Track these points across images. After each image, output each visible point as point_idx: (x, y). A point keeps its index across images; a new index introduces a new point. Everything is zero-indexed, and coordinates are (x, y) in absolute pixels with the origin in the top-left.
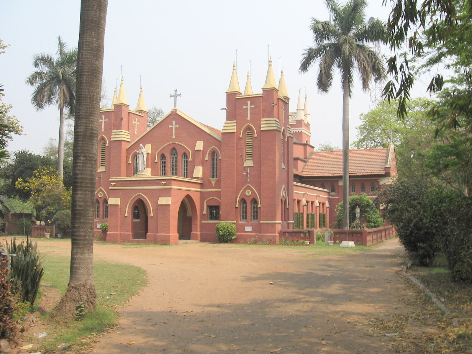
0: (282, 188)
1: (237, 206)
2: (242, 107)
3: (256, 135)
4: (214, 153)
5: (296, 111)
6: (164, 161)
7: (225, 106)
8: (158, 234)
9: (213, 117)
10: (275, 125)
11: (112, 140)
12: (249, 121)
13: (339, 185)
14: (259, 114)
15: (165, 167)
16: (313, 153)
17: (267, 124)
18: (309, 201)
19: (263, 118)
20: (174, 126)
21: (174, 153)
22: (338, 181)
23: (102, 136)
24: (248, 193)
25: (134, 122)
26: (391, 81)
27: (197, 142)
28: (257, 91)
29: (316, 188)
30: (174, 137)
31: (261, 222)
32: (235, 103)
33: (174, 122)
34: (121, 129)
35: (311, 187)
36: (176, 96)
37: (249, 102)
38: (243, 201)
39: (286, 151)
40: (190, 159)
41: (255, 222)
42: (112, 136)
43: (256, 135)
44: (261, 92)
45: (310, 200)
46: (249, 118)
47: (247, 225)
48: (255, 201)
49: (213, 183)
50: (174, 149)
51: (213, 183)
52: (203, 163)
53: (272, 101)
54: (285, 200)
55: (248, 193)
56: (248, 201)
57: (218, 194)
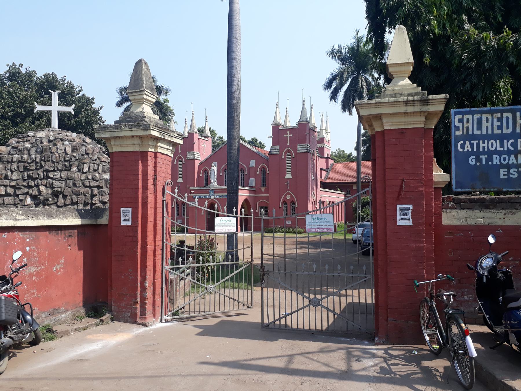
1: (281, 206)
3: (294, 156)
4: (263, 169)
12: (288, 146)
22: (352, 186)
24: (288, 197)
28: (293, 122)
29: (327, 190)
32: (278, 132)
35: (332, 191)
37: (288, 132)
38: (285, 203)
40: (246, 173)
45: (332, 201)
48: (294, 203)
49: (263, 189)
53: (304, 130)
56: (288, 203)
57: (267, 198)
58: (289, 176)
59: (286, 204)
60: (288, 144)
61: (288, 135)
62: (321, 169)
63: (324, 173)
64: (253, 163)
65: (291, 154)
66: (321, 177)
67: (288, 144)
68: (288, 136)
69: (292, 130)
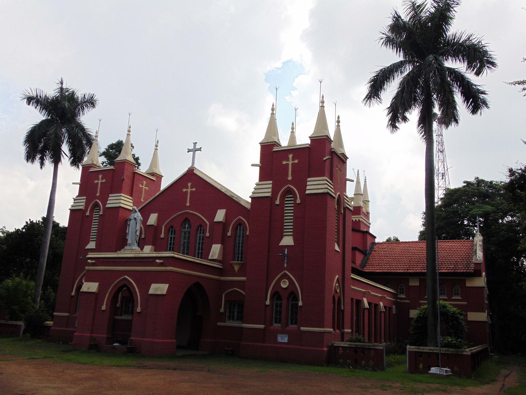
0: (334, 279)
1: (268, 302)
2: (281, 163)
3: (298, 201)
5: (353, 196)
6: (173, 236)
7: (258, 162)
8: (242, 343)
9: (242, 181)
10: (326, 186)
11: (107, 206)
13: (410, 285)
14: (304, 169)
15: (173, 244)
16: (374, 244)
17: (316, 185)
18: (372, 303)
19: (309, 177)
20: (189, 189)
21: (187, 226)
23: (97, 202)
25: (141, 186)
28: (303, 139)
30: (188, 204)
31: (302, 328)
32: (272, 158)
33: (189, 184)
34: (121, 193)
36: (195, 150)
37: (291, 156)
38: (277, 295)
39: (341, 227)
42: (108, 202)
43: (298, 201)
44: (309, 142)
47: (283, 332)
50: (186, 220)
51: (236, 268)
52: (223, 241)
53: (323, 156)
54: (339, 299)
55: (285, 284)
58: (287, 241)
59: (279, 298)
60: (290, 178)
61: (290, 162)
62: (354, 249)
63: (359, 257)
64: (220, 215)
65: (295, 197)
66: (354, 262)
67: (290, 178)
68: (290, 163)
69: (298, 152)
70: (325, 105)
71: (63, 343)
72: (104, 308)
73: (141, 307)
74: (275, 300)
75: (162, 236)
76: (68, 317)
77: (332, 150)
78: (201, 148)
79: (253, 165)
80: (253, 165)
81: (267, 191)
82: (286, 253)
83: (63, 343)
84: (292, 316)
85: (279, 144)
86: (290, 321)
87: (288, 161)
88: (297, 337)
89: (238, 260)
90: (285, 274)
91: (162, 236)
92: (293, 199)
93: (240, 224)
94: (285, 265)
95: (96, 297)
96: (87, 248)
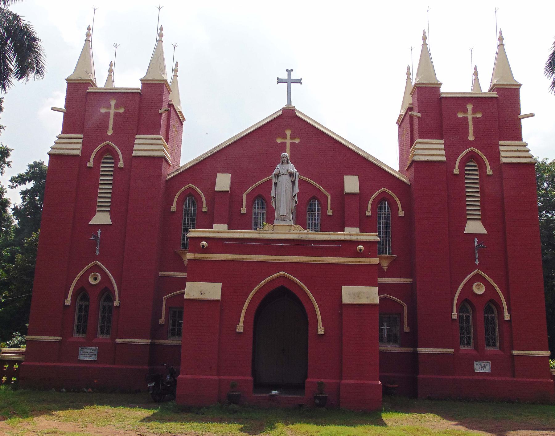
3: (121, 165)
24: (479, 289)
26: (20, 79)
27: (358, 176)
28: (130, 79)
37: (470, 107)
38: (83, 292)
41: (102, 337)
43: (121, 165)
44: (139, 85)
46: (110, 132)
55: (95, 279)
58: (102, 218)
59: (85, 298)
60: (471, 138)
61: (470, 114)
68: (112, 111)
69: (125, 97)
70: (504, 42)
71: (68, 391)
72: (240, 328)
73: (244, 323)
74: (78, 300)
75: (243, 210)
76: (60, 342)
77: (170, 103)
78: (301, 79)
79: (532, 115)
80: (532, 115)
81: (75, 146)
82: (99, 235)
83: (68, 391)
84: (79, 322)
85: (94, 84)
86: (99, 332)
87: (110, 109)
88: (506, 364)
89: (389, 253)
90: (96, 266)
91: (243, 210)
92: (112, 161)
93: (384, 197)
94: (477, 262)
95: (224, 308)
96: (92, 222)
